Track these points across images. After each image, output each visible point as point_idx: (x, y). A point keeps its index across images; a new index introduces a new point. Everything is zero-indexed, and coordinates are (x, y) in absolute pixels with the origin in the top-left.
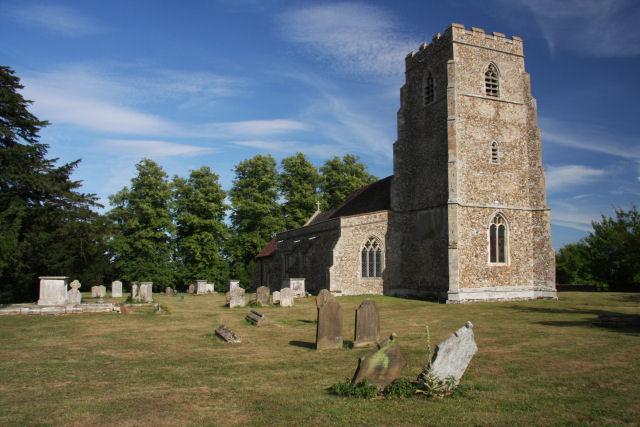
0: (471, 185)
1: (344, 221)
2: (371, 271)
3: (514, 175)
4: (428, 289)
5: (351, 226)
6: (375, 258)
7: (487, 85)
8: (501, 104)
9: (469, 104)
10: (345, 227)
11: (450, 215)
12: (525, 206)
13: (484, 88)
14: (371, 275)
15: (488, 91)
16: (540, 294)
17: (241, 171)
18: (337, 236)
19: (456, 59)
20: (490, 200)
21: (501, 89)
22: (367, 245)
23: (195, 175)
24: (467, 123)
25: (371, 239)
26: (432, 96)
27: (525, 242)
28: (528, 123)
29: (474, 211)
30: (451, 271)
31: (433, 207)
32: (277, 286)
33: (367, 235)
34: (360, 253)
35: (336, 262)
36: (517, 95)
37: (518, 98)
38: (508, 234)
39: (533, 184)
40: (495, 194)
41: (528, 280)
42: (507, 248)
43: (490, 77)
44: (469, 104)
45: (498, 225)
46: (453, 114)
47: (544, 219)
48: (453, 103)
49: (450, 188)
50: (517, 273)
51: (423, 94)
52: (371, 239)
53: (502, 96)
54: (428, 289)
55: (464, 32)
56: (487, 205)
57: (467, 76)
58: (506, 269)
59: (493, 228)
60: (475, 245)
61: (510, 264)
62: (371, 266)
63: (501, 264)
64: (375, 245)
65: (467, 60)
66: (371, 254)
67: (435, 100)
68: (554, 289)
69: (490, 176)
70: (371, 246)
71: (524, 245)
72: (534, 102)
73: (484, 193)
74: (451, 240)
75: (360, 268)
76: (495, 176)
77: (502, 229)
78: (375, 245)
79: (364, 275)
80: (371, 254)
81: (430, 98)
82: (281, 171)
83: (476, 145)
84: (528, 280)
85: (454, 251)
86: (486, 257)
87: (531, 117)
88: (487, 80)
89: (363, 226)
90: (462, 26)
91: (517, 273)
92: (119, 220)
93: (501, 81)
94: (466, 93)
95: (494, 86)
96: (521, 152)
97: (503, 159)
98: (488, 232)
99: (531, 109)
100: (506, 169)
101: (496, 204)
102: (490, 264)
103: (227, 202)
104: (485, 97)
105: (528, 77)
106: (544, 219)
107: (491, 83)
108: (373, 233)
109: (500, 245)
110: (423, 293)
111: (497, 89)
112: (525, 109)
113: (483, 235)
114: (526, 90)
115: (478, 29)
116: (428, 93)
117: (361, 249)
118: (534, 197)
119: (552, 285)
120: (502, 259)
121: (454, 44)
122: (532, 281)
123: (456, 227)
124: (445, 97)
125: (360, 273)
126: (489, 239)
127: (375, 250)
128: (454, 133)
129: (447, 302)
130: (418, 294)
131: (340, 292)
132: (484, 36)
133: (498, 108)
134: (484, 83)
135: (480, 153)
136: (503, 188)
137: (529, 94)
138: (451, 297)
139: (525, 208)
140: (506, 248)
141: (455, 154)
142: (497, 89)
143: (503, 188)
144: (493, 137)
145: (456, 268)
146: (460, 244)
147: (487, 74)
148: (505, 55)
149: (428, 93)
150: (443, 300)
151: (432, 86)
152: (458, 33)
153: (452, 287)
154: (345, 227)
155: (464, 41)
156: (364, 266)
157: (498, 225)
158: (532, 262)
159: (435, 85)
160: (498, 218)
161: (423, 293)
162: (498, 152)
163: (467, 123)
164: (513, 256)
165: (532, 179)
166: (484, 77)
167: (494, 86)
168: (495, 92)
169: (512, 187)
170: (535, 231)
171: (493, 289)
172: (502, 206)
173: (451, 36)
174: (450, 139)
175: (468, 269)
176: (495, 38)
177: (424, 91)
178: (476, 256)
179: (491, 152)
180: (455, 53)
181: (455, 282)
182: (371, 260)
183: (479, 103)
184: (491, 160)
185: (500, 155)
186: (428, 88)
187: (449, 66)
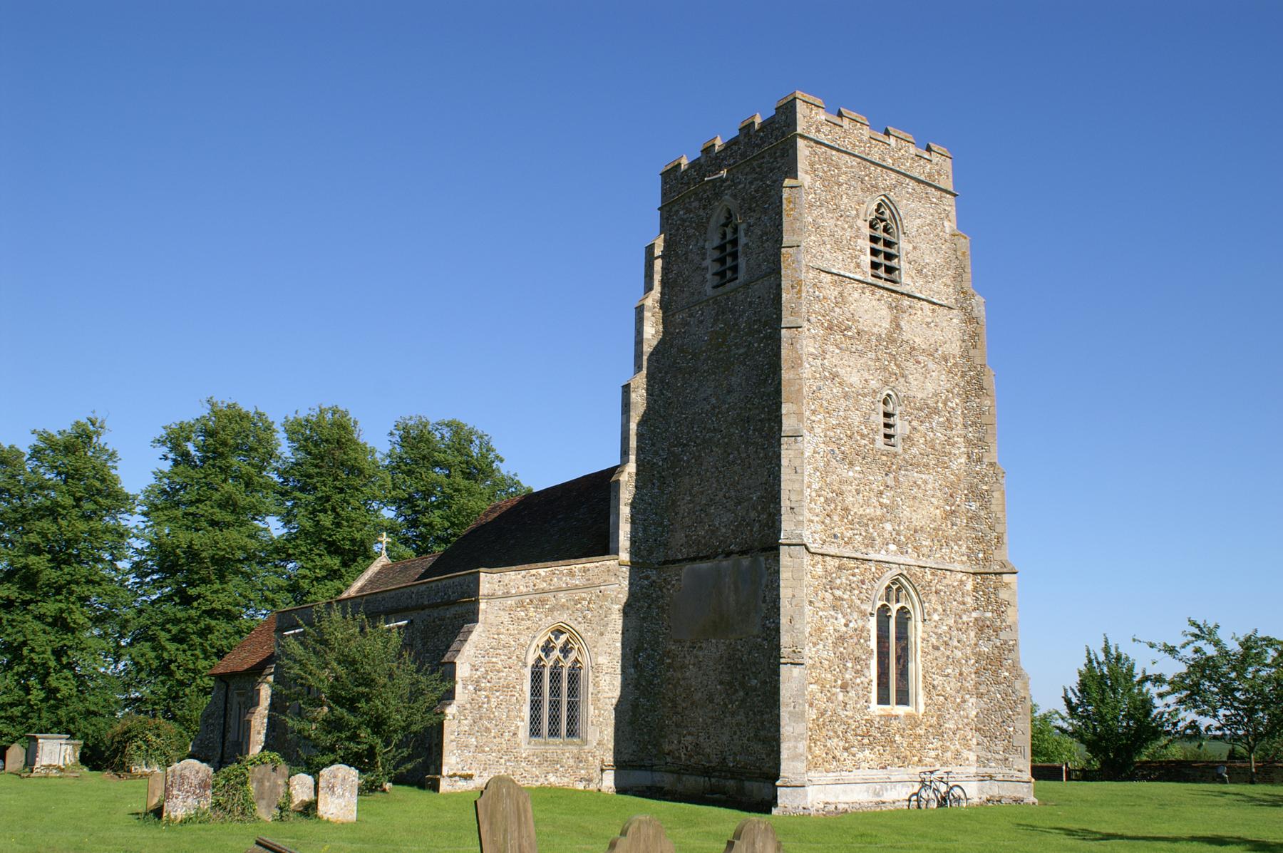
0: (835, 498)
1: (489, 581)
2: (554, 720)
3: (930, 480)
4: (706, 772)
5: (507, 595)
6: (565, 685)
7: (874, 252)
8: (906, 302)
9: (833, 293)
10: (491, 597)
11: (784, 575)
12: (957, 559)
13: (867, 259)
14: (554, 733)
15: (875, 266)
16: (994, 789)
17: (175, 441)
18: (471, 616)
19: (804, 177)
20: (878, 541)
21: (902, 264)
22: (547, 649)
23: (49, 448)
24: (825, 341)
25: (558, 632)
26: (735, 269)
27: (958, 654)
28: (966, 355)
29: (840, 568)
30: (788, 728)
31: (728, 555)
32: (1034, 796)
33: (550, 622)
34: (527, 672)
35: (462, 693)
36: (938, 285)
37: (942, 290)
38: (917, 632)
39: (974, 506)
40: (888, 527)
41: (965, 753)
42: (916, 667)
43: (880, 233)
44: (833, 293)
45: (894, 607)
46: (794, 312)
47: (1003, 595)
48: (797, 285)
49: (785, 504)
50: (940, 735)
51: (708, 262)
52: (558, 632)
53: (908, 281)
54: (706, 772)
55: (822, 116)
56: (873, 556)
57: (828, 223)
58: (913, 721)
59: (883, 613)
60: (842, 657)
61: (922, 709)
62: (555, 706)
63: (901, 710)
64: (565, 650)
65: (830, 183)
66: (556, 676)
67: (742, 276)
68: (1027, 775)
69: (877, 479)
70: (556, 653)
71: (956, 662)
72: (979, 305)
73: (865, 522)
74: (785, 639)
75: (526, 711)
76: (890, 482)
77: (903, 615)
78: (565, 650)
79: (535, 731)
80: (556, 676)
81: (726, 273)
82: (285, 449)
83: (846, 396)
84: (965, 753)
85: (796, 671)
86: (867, 689)
87: (972, 340)
88: (874, 239)
89: (539, 598)
90: (818, 102)
91: (940, 735)
92: (768, 186)
93: (904, 245)
94: (824, 265)
95: (889, 257)
96: (949, 425)
97: (907, 439)
98: (873, 624)
99: (971, 319)
100: (912, 464)
101: (889, 553)
102: (876, 709)
103: (133, 520)
104: (870, 279)
105: (964, 243)
106: (1003, 595)
107: (880, 246)
108: (563, 618)
109: (898, 659)
110: (691, 782)
111: (894, 263)
112: (956, 317)
113: (861, 633)
114: (958, 276)
115: (854, 115)
116: (722, 261)
117: (531, 662)
118: (979, 540)
119: (1023, 765)
120: (903, 699)
121: (801, 143)
122: (972, 757)
123: (800, 607)
124: (776, 271)
125: (524, 726)
126: (873, 644)
127: (567, 664)
128: (797, 364)
129: (774, 811)
130: (680, 787)
131: (468, 777)
132: (866, 132)
133: (896, 309)
134: (867, 245)
135: (856, 418)
136: (907, 512)
137: (967, 286)
138: (785, 798)
139: (959, 567)
140: (911, 666)
141: (800, 415)
142: (894, 263)
143: (907, 512)
144: (886, 383)
145: (799, 717)
146: (808, 652)
147: (872, 226)
148: (912, 183)
149: (722, 261)
150: (766, 804)
151: (734, 242)
152: (809, 118)
153: (788, 768)
154: (491, 597)
155: (821, 138)
156: (536, 706)
157: (894, 607)
158: (972, 707)
159: (743, 240)
160: (896, 589)
161: (691, 782)
162: (895, 420)
163: (825, 341)
164: (930, 688)
165: (975, 493)
166: (867, 231)
167: (889, 257)
168: (890, 270)
169: (926, 513)
170: (981, 627)
171: (881, 774)
172: (901, 559)
173: (793, 123)
174: (786, 375)
175: (825, 722)
176: (892, 141)
177: (712, 254)
178: (844, 687)
179: (882, 420)
180: (802, 164)
181: (795, 757)
182: (555, 691)
183: (854, 292)
184: (880, 440)
185: (901, 427)
186: (721, 248)
187: (786, 194)
